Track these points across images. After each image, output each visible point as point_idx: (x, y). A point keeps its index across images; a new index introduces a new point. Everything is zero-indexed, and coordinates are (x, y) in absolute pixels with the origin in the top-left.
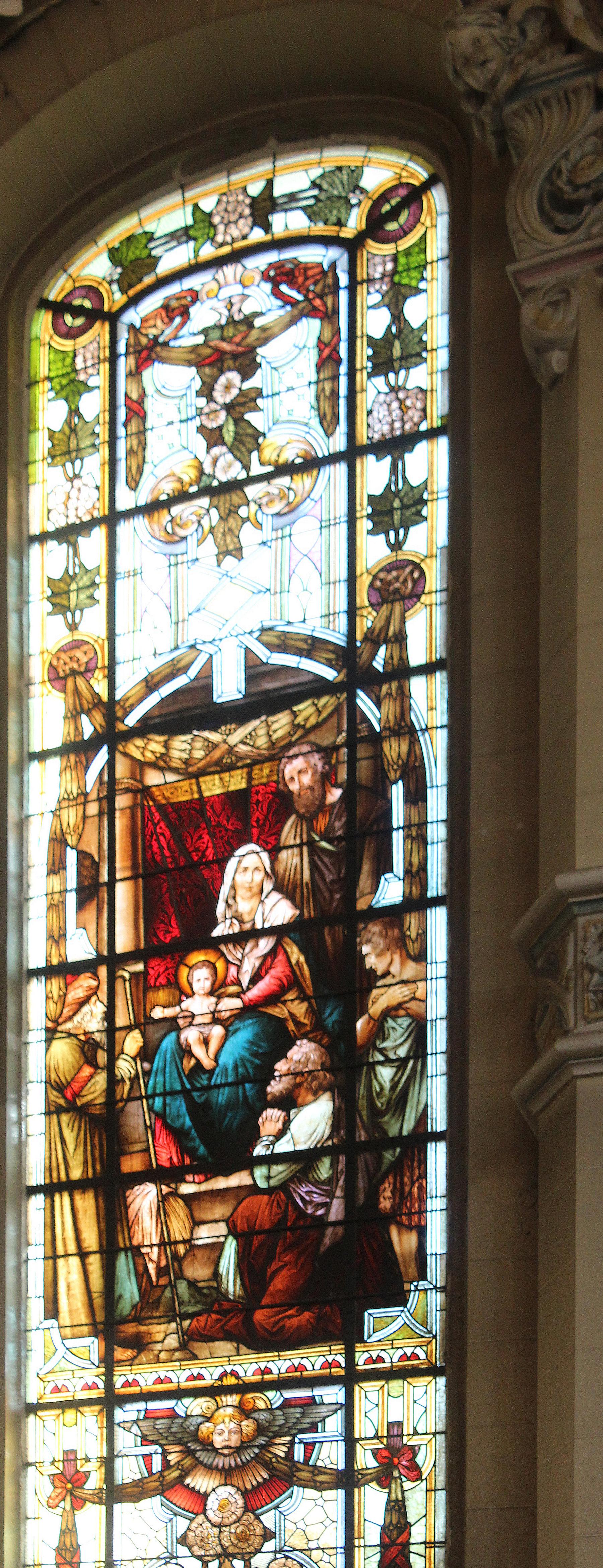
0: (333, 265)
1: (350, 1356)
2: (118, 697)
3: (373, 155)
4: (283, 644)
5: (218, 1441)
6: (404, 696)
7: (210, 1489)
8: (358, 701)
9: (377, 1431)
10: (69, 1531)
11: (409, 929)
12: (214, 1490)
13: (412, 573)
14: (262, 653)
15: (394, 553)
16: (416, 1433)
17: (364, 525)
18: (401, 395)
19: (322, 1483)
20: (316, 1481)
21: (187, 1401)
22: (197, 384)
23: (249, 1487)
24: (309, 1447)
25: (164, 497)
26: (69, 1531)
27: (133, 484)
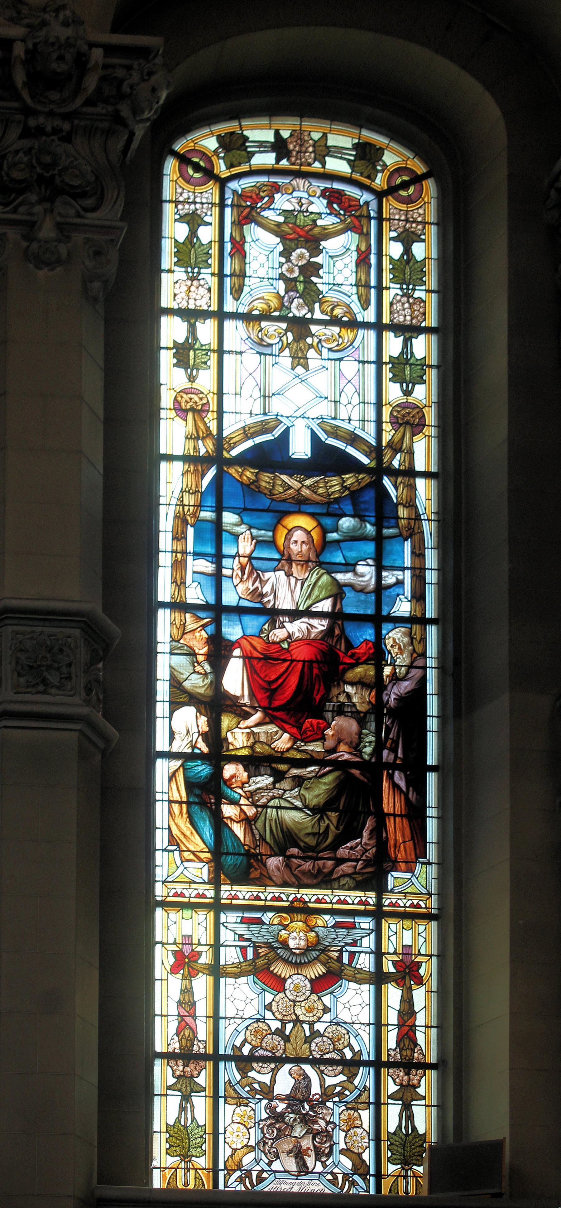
0: (367, 203)
1: (379, 898)
2: (225, 434)
3: (393, 145)
4: (335, 432)
5: (292, 944)
6: (413, 488)
7: (287, 976)
8: (384, 481)
9: (396, 949)
10: (187, 991)
11: (415, 634)
12: (290, 976)
13: (418, 413)
14: (323, 436)
15: (405, 397)
16: (420, 954)
17: (387, 374)
18: (411, 300)
19: (360, 979)
20: (356, 978)
21: (270, 915)
22: (281, 248)
23: (313, 977)
24: (352, 955)
25: (256, 312)
26: (187, 991)
27: (237, 292)
